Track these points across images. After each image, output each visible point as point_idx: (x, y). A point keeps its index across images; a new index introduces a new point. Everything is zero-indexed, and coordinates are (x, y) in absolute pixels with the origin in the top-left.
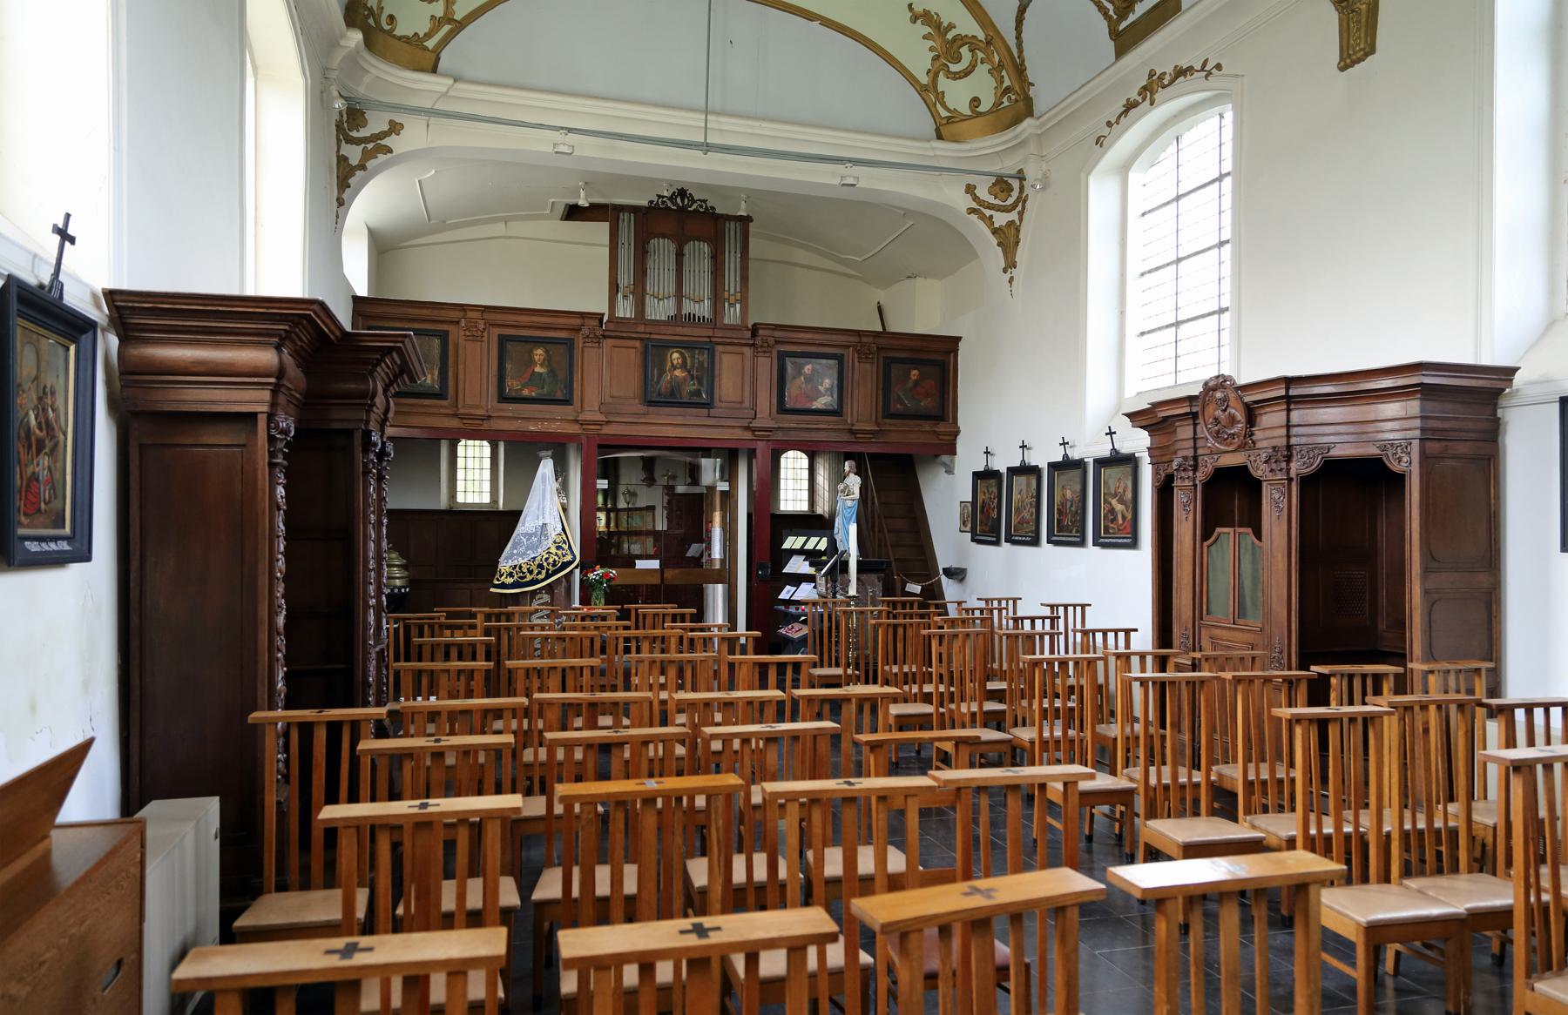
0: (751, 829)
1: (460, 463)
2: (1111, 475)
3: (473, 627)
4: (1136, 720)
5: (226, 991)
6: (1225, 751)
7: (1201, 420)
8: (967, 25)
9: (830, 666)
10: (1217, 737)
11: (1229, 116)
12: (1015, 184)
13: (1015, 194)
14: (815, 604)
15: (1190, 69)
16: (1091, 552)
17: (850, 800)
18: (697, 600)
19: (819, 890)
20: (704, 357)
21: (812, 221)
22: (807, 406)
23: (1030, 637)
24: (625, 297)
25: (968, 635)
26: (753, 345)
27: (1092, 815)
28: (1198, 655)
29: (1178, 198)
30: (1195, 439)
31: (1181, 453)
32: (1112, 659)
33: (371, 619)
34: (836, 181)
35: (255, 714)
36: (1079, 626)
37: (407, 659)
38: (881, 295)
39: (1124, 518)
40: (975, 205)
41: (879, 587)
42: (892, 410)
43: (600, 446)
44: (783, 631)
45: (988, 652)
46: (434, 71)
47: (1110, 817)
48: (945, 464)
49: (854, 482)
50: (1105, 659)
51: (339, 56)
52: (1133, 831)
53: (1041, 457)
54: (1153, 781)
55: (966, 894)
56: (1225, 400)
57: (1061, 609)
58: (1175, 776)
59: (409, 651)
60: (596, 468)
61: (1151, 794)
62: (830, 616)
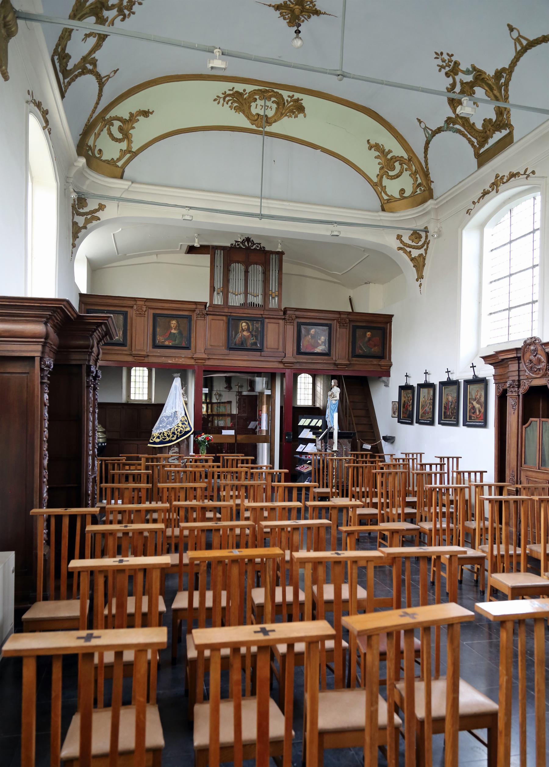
0: (284, 573)
1: (133, 379)
2: (472, 388)
3: (140, 465)
4: (487, 519)
5: (29, 657)
6: (534, 537)
7: (522, 361)
8: (398, 151)
9: (323, 487)
10: (530, 529)
11: (539, 198)
12: (423, 234)
13: (423, 240)
14: (315, 455)
15: (518, 174)
16: (462, 429)
17: (337, 562)
18: (253, 451)
19: (321, 608)
20: (259, 325)
21: (317, 255)
22: (312, 351)
23: (430, 475)
24: (218, 294)
25: (397, 473)
26: (284, 319)
27: (462, 570)
28: (519, 486)
29: (511, 242)
30: (519, 371)
31: (511, 378)
32: (473, 488)
33: (90, 461)
34: (329, 233)
35: (32, 511)
36: (455, 469)
37: (106, 482)
38: (351, 293)
39: (480, 411)
40: (402, 246)
41: (349, 446)
42: (357, 353)
43: (204, 371)
44: (298, 468)
45: (406, 482)
46: (121, 178)
47: (472, 571)
48: (384, 382)
49: (336, 391)
50: (469, 488)
51: (74, 171)
52: (484, 579)
53: (436, 379)
54: (495, 553)
55: (401, 616)
56: (536, 350)
57: (446, 460)
58: (507, 550)
59: (106, 477)
60: (202, 382)
61: (494, 559)
62: (323, 461)
